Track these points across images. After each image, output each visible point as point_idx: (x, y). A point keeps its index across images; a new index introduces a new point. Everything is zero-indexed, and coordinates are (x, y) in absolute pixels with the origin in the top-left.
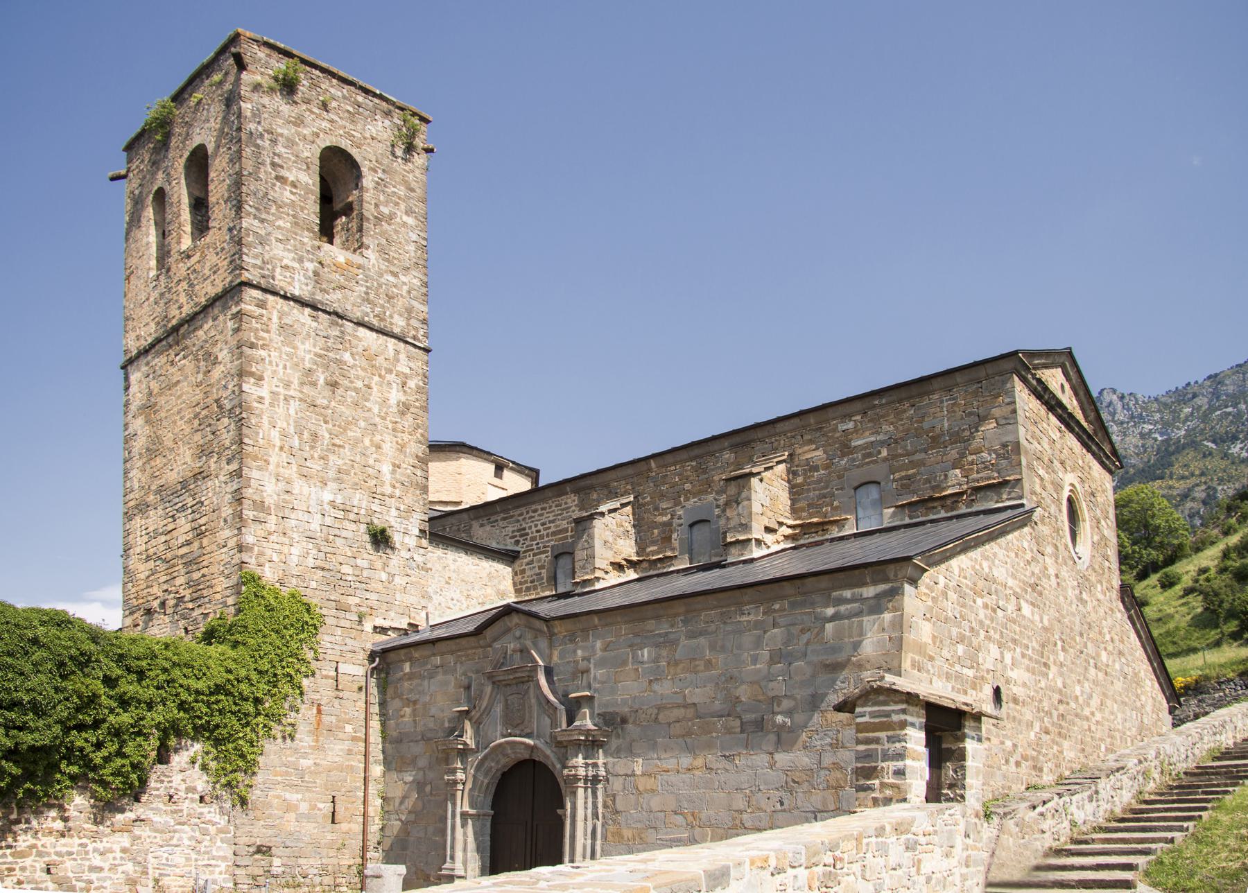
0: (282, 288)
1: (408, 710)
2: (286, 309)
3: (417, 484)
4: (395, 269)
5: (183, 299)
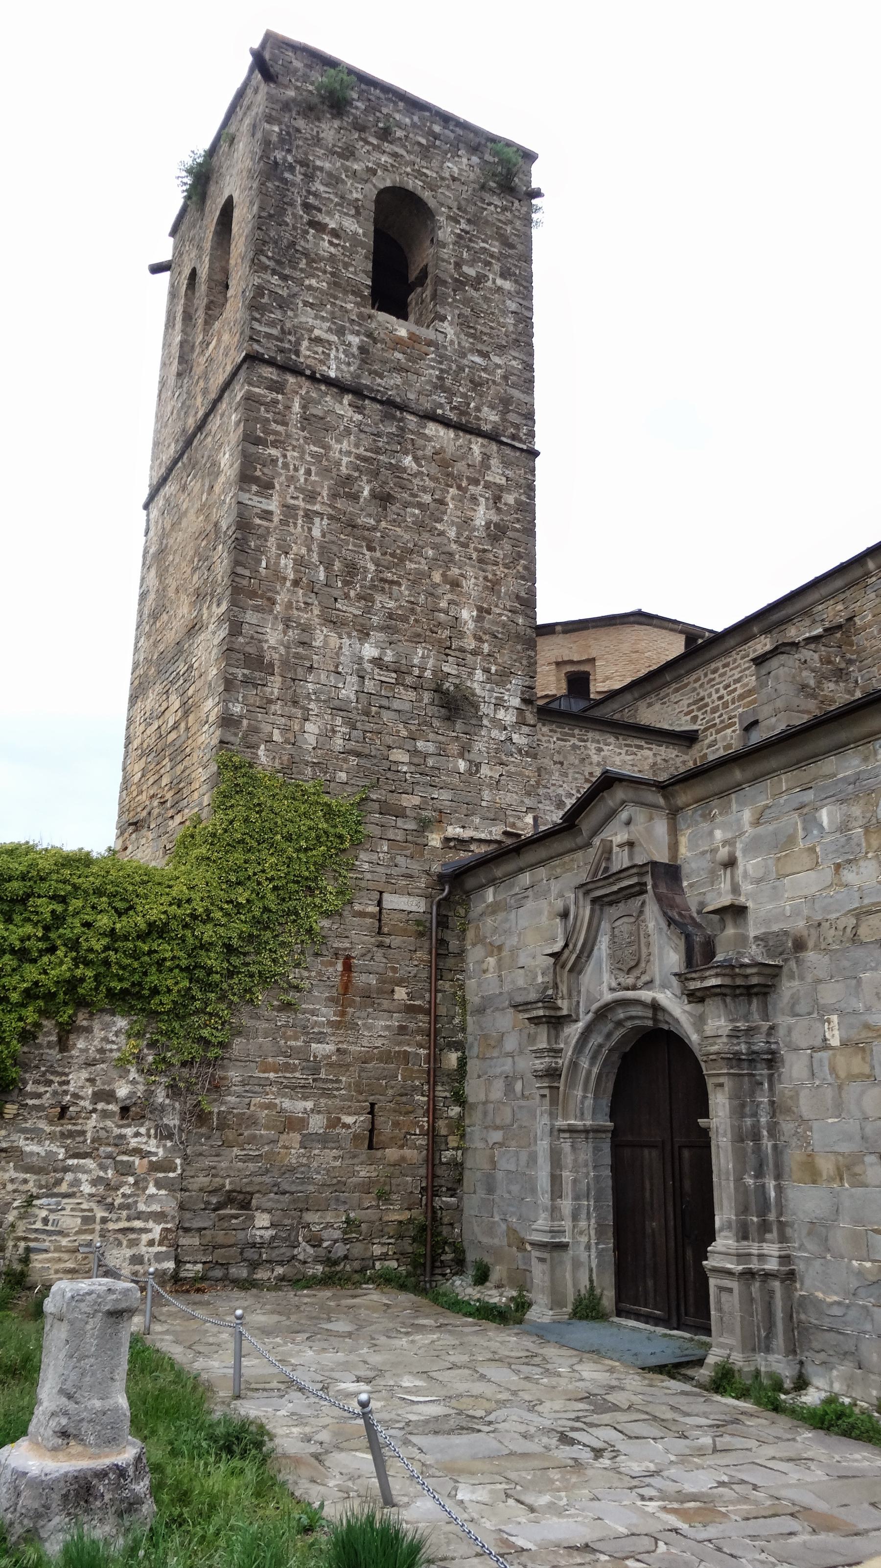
4: (485, 349)
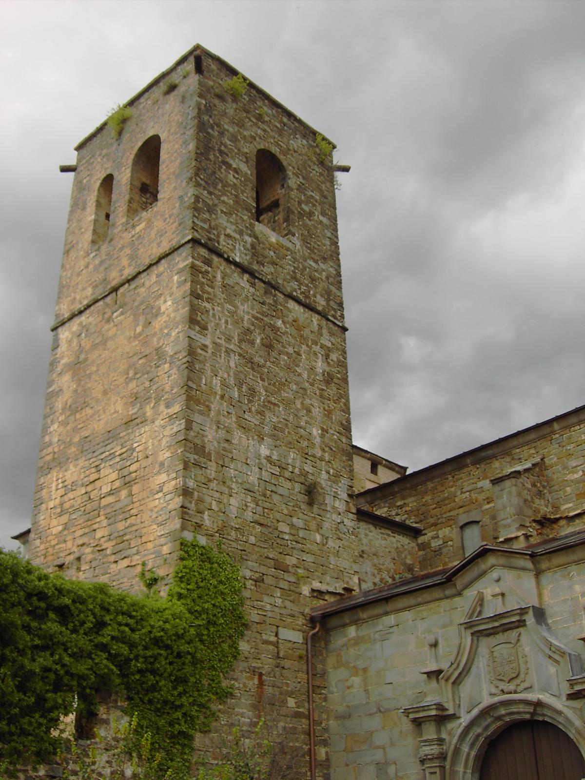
0: (225, 252)
1: (357, 680)
2: (228, 271)
3: (343, 450)
5: (125, 262)
